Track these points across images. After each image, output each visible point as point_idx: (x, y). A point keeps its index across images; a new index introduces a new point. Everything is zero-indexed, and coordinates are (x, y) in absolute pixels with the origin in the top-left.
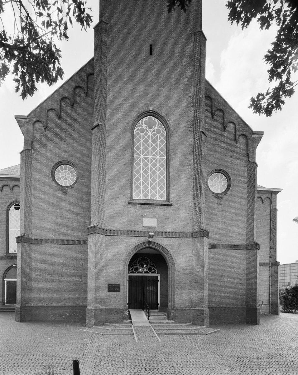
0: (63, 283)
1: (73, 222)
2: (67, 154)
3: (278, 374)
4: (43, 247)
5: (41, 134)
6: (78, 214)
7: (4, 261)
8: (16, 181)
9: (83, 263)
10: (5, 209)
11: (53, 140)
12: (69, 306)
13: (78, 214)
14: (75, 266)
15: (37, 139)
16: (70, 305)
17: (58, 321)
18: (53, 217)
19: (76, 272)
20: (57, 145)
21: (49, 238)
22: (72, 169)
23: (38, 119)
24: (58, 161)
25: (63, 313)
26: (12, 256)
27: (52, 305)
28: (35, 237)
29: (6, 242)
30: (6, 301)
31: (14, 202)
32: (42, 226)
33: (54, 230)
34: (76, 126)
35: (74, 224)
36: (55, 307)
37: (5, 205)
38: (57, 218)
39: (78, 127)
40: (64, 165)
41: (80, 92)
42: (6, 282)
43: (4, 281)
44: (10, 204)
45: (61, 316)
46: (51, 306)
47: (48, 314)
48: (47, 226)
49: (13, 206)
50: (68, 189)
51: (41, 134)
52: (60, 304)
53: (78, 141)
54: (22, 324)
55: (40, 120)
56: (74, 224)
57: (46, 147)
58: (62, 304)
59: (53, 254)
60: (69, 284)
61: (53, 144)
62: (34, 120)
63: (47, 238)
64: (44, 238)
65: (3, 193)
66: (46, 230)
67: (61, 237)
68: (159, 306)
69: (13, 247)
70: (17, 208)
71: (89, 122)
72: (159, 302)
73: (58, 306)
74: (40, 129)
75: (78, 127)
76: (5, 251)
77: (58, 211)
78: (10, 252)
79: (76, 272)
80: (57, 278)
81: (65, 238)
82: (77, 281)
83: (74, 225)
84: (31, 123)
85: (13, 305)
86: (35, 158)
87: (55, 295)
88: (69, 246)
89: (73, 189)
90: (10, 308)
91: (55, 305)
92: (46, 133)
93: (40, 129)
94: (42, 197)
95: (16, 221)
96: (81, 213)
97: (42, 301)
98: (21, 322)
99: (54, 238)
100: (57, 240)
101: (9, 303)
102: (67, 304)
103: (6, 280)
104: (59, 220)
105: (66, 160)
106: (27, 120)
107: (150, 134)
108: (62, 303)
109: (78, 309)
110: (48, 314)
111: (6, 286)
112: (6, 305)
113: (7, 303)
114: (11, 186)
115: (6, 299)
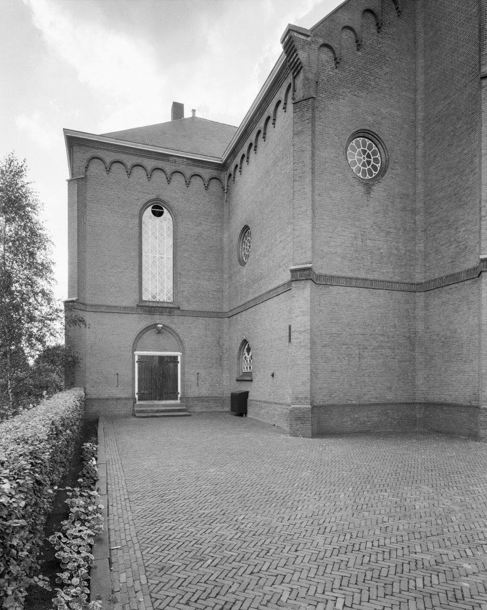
0: (366, 360)
1: (380, 246)
2: (370, 119)
3: (7, 486)
4: (335, 290)
5: (330, 73)
6: (388, 233)
7: (135, 315)
8: (158, 159)
9: (396, 323)
10: (137, 212)
11: (349, 88)
12: (377, 404)
13: (388, 233)
14: (385, 328)
15: (323, 80)
16: (377, 401)
17: (360, 432)
18: (350, 235)
19: (386, 340)
20: (355, 97)
21: (344, 275)
22: (374, 149)
23: (326, 42)
24: (357, 130)
25: (367, 417)
26: (152, 307)
27: (349, 402)
28: (321, 271)
29: (137, 279)
30: (137, 396)
31: (154, 200)
32: (331, 250)
33: (351, 261)
34: (384, 68)
35: (382, 251)
36: (355, 405)
37: (137, 205)
38: (356, 238)
39: (388, 70)
40: (362, 139)
41: (390, 5)
42: (136, 359)
43: (134, 356)
44: (146, 204)
45: (365, 422)
46: (349, 405)
47: (345, 420)
48: (339, 250)
49: (149, 209)
50: (373, 185)
51: (330, 73)
52: (362, 401)
53: (388, 96)
54: (317, 441)
55: (330, 43)
56: (382, 251)
57: (338, 99)
58: (365, 399)
59: (349, 306)
60: (374, 362)
61: (349, 95)
62: (321, 41)
63: (340, 274)
64: (335, 273)
65: (131, 179)
66: (338, 259)
67: (362, 275)
68: (179, 396)
69: (150, 290)
70: (158, 213)
71: (404, 64)
72: (179, 390)
73: (359, 405)
74: (327, 62)
75: (388, 70)
76: (136, 297)
77: (357, 224)
78: (144, 298)
79: (386, 340)
80: (357, 352)
81: (370, 277)
82: (387, 356)
83: (381, 253)
84: (316, 47)
85: (151, 403)
86: (320, 118)
87: (354, 382)
88: (374, 291)
89: (381, 185)
90: (158, 408)
91: (354, 402)
92: (337, 71)
93: (327, 62)
94: (331, 193)
95: (156, 238)
96: (392, 231)
97: (333, 396)
98: (313, 437)
99: (351, 275)
100: (357, 279)
101: (144, 400)
102: (373, 401)
103: (136, 353)
104: (359, 243)
105: (367, 128)
106: (309, 39)
108: (366, 398)
109: (391, 410)
110: (345, 420)
111: (136, 365)
112: (138, 403)
113: (139, 400)
114: (149, 169)
115: (136, 391)
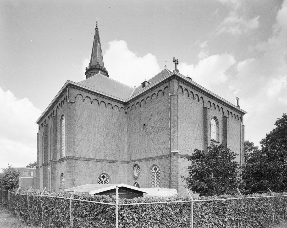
107: (104, 181)
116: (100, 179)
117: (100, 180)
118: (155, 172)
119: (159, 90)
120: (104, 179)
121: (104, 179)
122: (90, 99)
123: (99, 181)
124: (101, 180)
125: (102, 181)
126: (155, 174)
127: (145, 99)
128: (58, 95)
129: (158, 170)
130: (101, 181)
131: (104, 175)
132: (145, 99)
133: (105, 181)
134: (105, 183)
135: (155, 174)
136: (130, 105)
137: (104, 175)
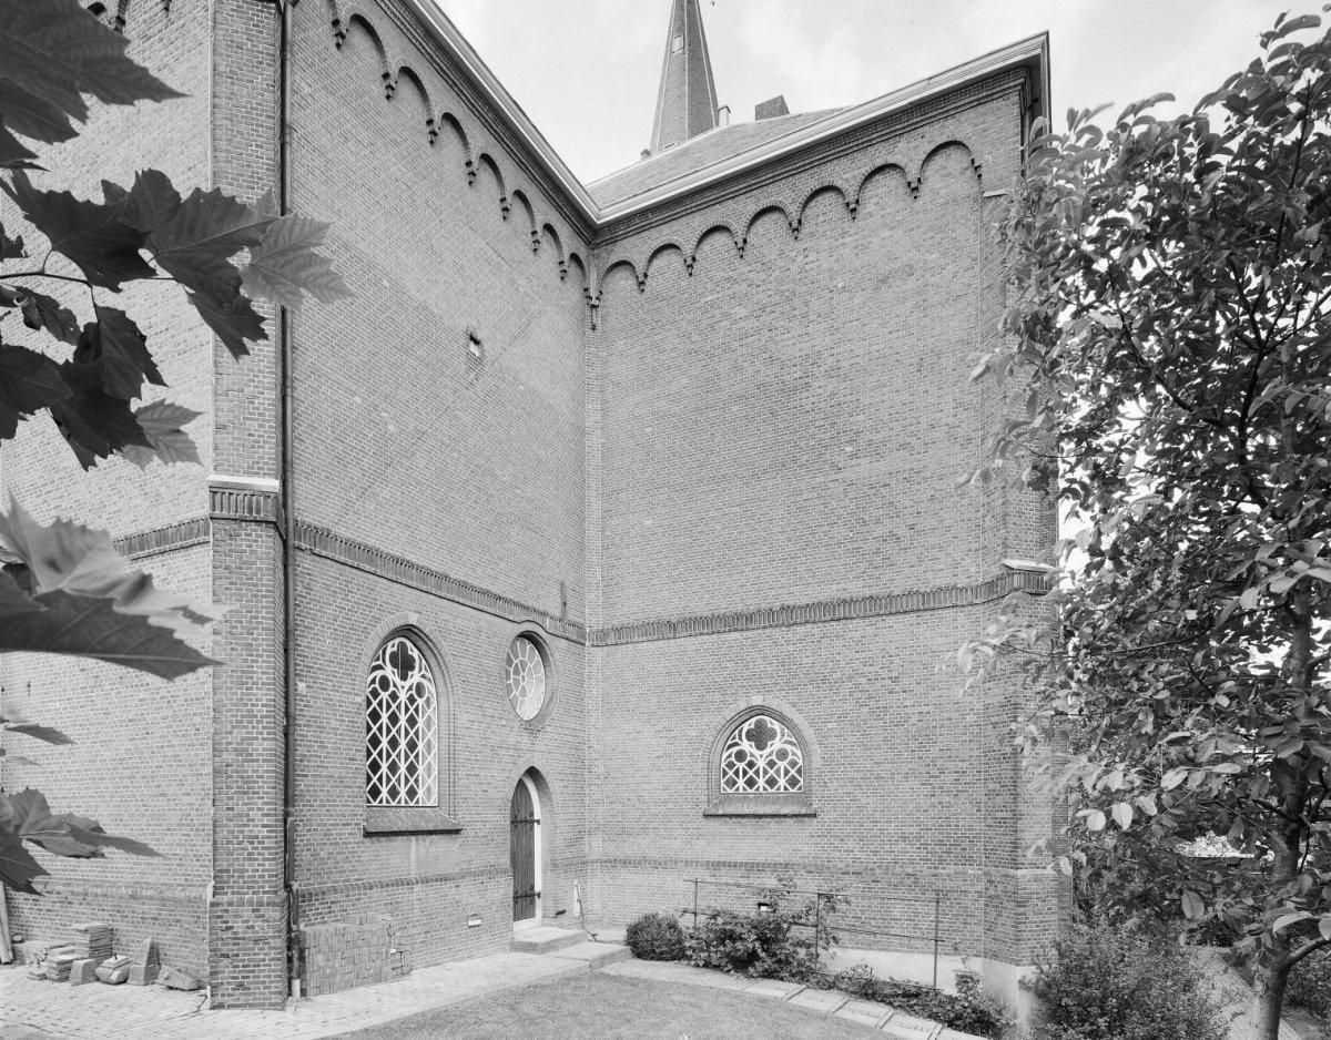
107: (761, 764)
116: (735, 749)
117: (733, 759)
118: (399, 682)
119: (814, 185)
120: (761, 746)
121: (761, 746)
122: (415, 91)
123: (731, 765)
124: (740, 756)
125: (751, 765)
126: (403, 697)
127: (738, 227)
128: (947, 80)
129: (423, 676)
130: (741, 766)
131: (760, 725)
132: (738, 227)
133: (771, 764)
134: (731, 773)
135: (403, 697)
136: (635, 248)
137: (760, 725)
